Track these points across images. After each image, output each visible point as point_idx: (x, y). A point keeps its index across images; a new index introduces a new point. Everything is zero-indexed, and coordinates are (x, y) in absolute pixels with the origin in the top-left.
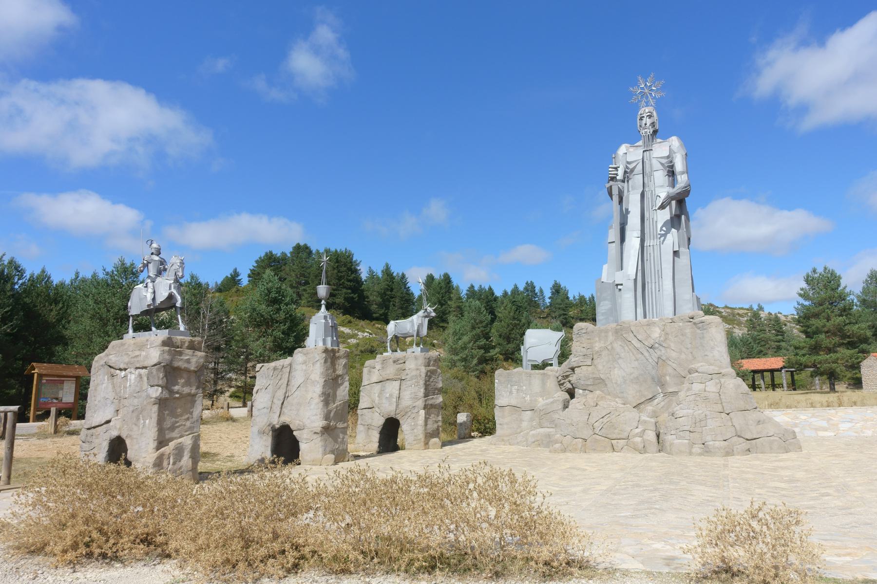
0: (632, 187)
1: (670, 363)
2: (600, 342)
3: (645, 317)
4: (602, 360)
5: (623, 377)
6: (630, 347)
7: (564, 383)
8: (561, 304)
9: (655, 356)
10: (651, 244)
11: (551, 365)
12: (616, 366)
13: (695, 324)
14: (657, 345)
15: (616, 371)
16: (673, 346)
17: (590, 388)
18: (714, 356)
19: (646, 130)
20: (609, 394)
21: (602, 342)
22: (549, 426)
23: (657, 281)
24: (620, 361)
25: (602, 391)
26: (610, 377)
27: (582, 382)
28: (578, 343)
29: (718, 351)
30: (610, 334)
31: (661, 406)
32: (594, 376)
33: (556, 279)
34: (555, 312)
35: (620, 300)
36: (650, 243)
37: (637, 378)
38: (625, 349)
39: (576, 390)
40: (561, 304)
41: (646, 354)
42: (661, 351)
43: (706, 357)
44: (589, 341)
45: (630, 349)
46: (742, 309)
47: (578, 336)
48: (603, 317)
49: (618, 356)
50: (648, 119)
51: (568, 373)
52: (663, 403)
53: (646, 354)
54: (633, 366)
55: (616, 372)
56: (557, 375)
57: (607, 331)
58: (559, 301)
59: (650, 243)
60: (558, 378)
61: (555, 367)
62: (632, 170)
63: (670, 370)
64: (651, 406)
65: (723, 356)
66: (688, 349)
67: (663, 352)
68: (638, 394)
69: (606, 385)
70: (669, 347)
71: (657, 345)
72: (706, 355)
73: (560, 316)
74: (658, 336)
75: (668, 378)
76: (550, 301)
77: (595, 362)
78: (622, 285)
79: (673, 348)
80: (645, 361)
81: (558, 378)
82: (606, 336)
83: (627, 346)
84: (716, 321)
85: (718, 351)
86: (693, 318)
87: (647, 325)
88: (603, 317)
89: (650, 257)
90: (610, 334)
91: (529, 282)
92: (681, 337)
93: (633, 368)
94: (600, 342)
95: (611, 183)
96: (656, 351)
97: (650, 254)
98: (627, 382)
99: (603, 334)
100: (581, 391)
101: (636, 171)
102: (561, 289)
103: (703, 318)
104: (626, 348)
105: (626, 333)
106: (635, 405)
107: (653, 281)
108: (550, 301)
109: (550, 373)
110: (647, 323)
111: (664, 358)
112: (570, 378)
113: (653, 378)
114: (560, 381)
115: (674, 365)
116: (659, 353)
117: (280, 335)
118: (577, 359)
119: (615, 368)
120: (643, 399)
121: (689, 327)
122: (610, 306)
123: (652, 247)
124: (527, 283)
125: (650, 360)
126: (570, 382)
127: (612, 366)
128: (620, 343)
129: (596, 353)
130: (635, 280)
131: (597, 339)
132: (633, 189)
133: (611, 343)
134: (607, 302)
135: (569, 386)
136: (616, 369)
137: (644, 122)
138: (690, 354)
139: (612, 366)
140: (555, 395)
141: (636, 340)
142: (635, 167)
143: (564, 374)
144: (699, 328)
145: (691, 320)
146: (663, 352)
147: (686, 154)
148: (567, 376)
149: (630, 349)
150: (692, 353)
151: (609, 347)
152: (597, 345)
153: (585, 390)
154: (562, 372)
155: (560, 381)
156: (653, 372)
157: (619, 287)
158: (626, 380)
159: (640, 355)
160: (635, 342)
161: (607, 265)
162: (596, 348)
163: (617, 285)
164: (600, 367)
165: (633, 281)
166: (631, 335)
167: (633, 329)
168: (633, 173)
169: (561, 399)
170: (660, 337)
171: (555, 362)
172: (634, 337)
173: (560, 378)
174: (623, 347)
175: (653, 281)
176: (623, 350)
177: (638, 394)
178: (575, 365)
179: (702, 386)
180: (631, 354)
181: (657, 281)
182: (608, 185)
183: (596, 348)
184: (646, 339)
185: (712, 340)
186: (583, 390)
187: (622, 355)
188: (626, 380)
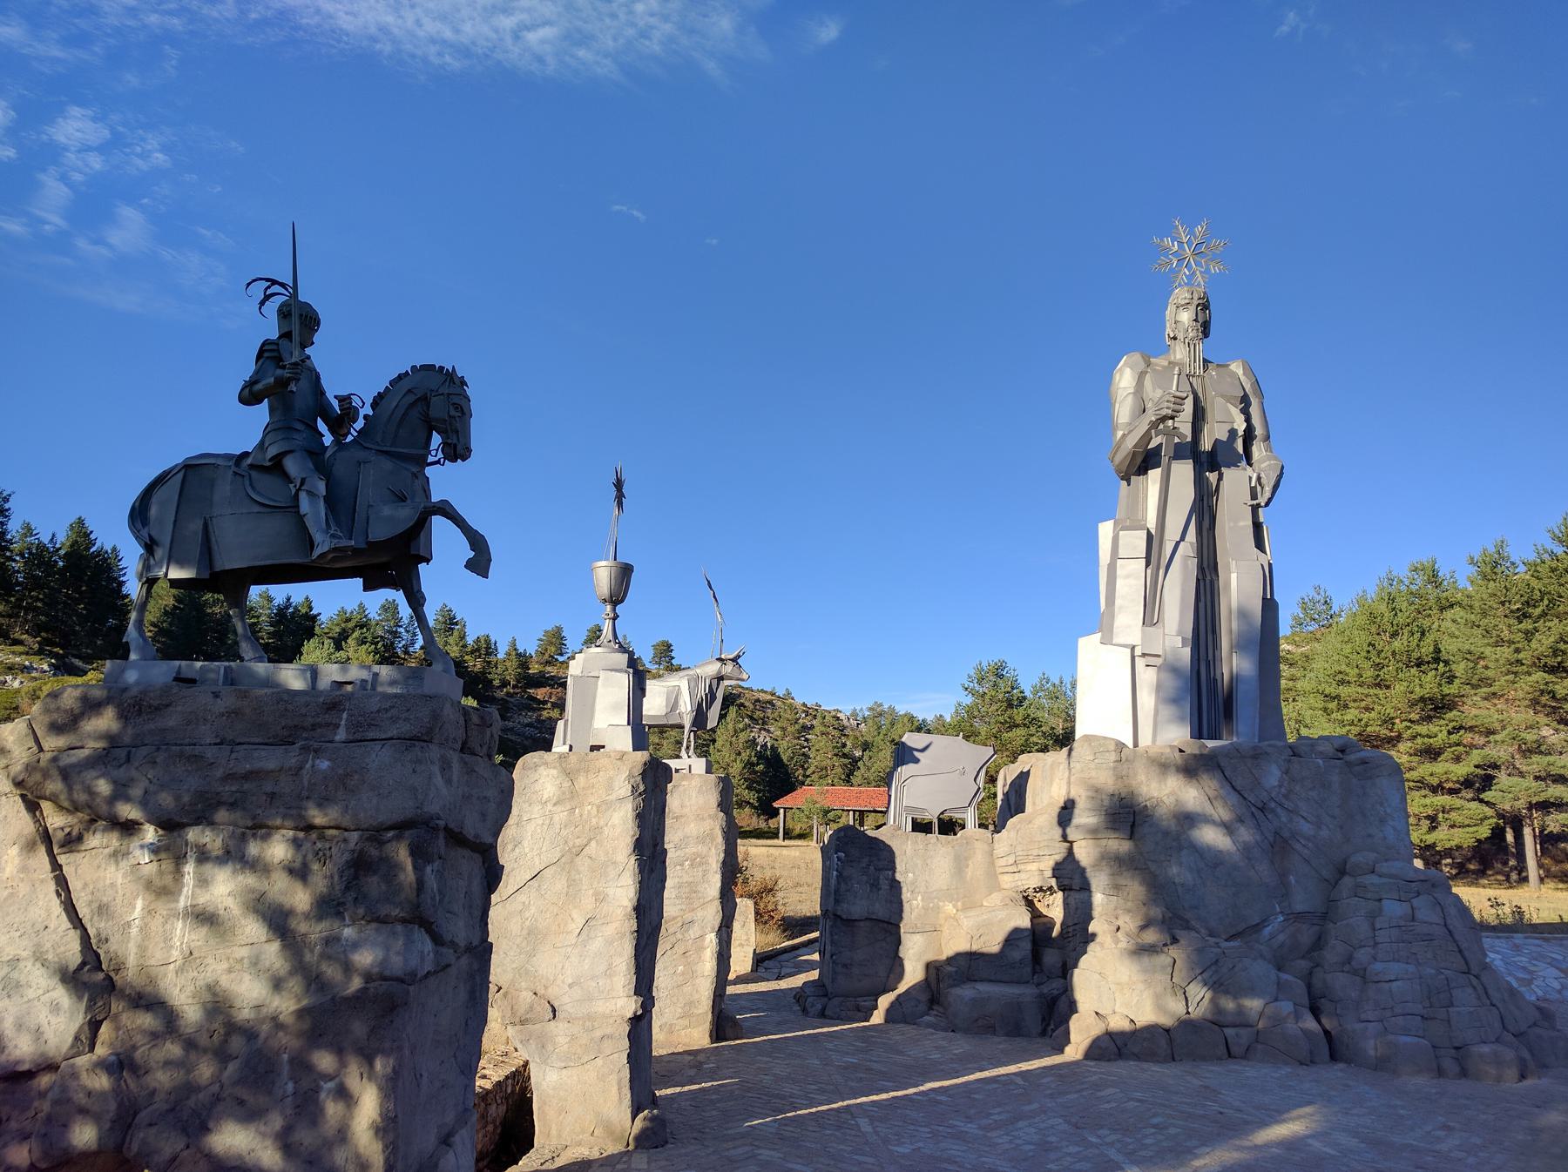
13: (1349, 764)
22: (992, 978)
29: (1394, 829)
46: (762, 691)
66: (1334, 817)
72: (1370, 836)
74: (1276, 784)
79: (1305, 814)
85: (1394, 829)
96: (1270, 816)
185: (1382, 804)
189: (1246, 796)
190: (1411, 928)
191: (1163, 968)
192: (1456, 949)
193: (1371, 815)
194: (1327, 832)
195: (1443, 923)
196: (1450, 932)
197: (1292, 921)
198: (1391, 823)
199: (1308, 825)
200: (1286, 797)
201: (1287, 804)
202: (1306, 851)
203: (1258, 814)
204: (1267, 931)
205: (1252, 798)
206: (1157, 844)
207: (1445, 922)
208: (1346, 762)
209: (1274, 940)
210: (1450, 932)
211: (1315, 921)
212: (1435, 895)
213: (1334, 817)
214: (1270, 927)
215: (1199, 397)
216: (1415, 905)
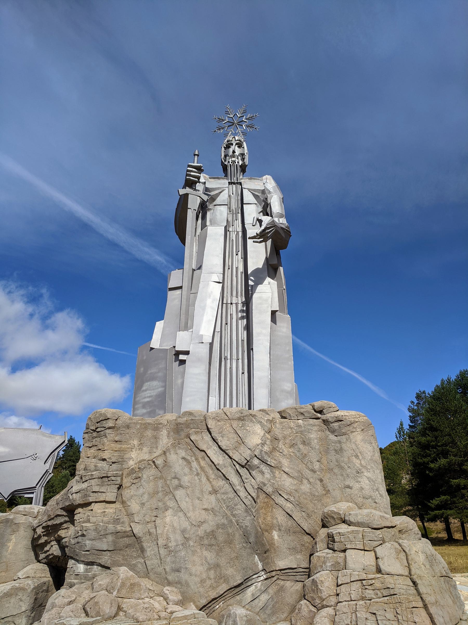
0: (210, 221)
1: (280, 501)
2: (141, 449)
3: (237, 406)
4: (141, 491)
5: (183, 531)
6: (203, 463)
7: (46, 543)
8: (72, 457)
9: (251, 484)
10: (234, 302)
11: (30, 501)
12: (171, 503)
13: (326, 422)
14: (256, 462)
15: (169, 517)
16: (285, 463)
17: (105, 559)
18: (362, 489)
19: (233, 159)
20: (147, 575)
21: (145, 449)
23: (240, 357)
24: (179, 493)
25: (132, 568)
26: (153, 530)
27: (88, 544)
28: (93, 450)
29: (368, 478)
30: (164, 432)
31: (261, 604)
32: (119, 528)
33: (72, 435)
34: (66, 463)
35: (179, 381)
36: (231, 300)
37: (212, 534)
38: (191, 468)
39: (71, 563)
40: (72, 457)
41: (234, 479)
42: (263, 473)
43: (348, 490)
44: (118, 446)
45: (201, 468)
47: (95, 434)
48: (144, 411)
49: (176, 482)
50: (237, 148)
51: (58, 521)
52: (264, 598)
53: (234, 479)
54: (205, 507)
55: (168, 520)
56: (35, 523)
57: (157, 428)
58: (71, 453)
59: (231, 300)
60: (34, 530)
61: (36, 508)
62: (213, 199)
63: (281, 518)
64: (239, 603)
65: (377, 490)
66: (314, 471)
67: (267, 476)
68: (212, 574)
69: (142, 550)
70: (278, 467)
71: (256, 462)
72: (349, 487)
73: (69, 467)
74: (260, 441)
75: (275, 535)
76: (63, 453)
77: (126, 493)
78: (187, 353)
79: (286, 470)
80: (232, 495)
81: (34, 530)
82: (156, 438)
83: (197, 459)
84: (361, 419)
85: (368, 478)
86: (321, 412)
87: (240, 419)
88: (144, 411)
89: (231, 318)
90: (164, 432)
92: (301, 446)
93: (205, 509)
94: (141, 449)
95: (188, 190)
96: (253, 473)
97: (231, 315)
98: (191, 543)
99: (149, 433)
100: (81, 568)
101: (218, 201)
102: (76, 444)
103: (339, 413)
104: (195, 464)
105: (196, 433)
106: (204, 602)
107: (235, 357)
108: (63, 453)
109: (21, 519)
110: (237, 416)
111: (269, 489)
112: (62, 533)
113: (246, 535)
114: (40, 537)
115: (288, 506)
116: (259, 478)
117: (181, 553)
118: (85, 485)
119: (166, 509)
120: (223, 588)
121: (316, 428)
122: (160, 389)
123: (234, 305)
125: (242, 494)
126: (59, 540)
127: (160, 504)
128: (182, 453)
129: (129, 475)
130: (211, 344)
131: (136, 442)
132: (213, 223)
133: (165, 453)
134: (155, 383)
135: (55, 550)
136: (170, 512)
137: (231, 150)
138: (318, 482)
139: (160, 504)
140: (20, 574)
141: (217, 448)
142: (218, 195)
143: (50, 523)
144: (333, 431)
145: (319, 415)
146: (267, 476)
147: (283, 198)
148: (57, 527)
149: (201, 468)
150: (321, 480)
151: (159, 462)
152: (134, 454)
153: (92, 563)
154: (45, 518)
155: (40, 537)
156: (247, 522)
157: (182, 357)
158: (187, 539)
159: (222, 482)
160: (213, 452)
161: (162, 322)
162: (131, 463)
163: (178, 353)
164: (134, 506)
165: (208, 346)
166: (207, 437)
167: (211, 424)
168: (215, 203)
169: (30, 584)
170: (263, 444)
171: (39, 494)
172: (211, 443)
173: (40, 531)
174: (188, 462)
175: (235, 357)
176: (187, 470)
177: (212, 574)
178: (77, 499)
179: (369, 559)
180: (204, 479)
181: (240, 357)
182: (182, 192)
183: (131, 463)
184: (235, 448)
185: (357, 456)
186: (88, 564)
187: (186, 480)
188: (187, 539)
189: (231, 455)
190: (370, 582)
191: (441, 573)
192: (420, 604)
193: (349, 467)
194: (308, 486)
195: (407, 573)
196: (414, 583)
197: (275, 578)
198: (368, 475)
199: (291, 480)
200: (269, 454)
201: (270, 461)
202: (289, 505)
203: (243, 471)
204: (250, 592)
205: (236, 456)
206: (143, 504)
207: (410, 573)
208: (324, 420)
209: (256, 601)
210: (414, 583)
211: (298, 578)
212: (400, 541)
213: (314, 471)
214: (253, 588)
215: (241, 160)
216: (379, 555)
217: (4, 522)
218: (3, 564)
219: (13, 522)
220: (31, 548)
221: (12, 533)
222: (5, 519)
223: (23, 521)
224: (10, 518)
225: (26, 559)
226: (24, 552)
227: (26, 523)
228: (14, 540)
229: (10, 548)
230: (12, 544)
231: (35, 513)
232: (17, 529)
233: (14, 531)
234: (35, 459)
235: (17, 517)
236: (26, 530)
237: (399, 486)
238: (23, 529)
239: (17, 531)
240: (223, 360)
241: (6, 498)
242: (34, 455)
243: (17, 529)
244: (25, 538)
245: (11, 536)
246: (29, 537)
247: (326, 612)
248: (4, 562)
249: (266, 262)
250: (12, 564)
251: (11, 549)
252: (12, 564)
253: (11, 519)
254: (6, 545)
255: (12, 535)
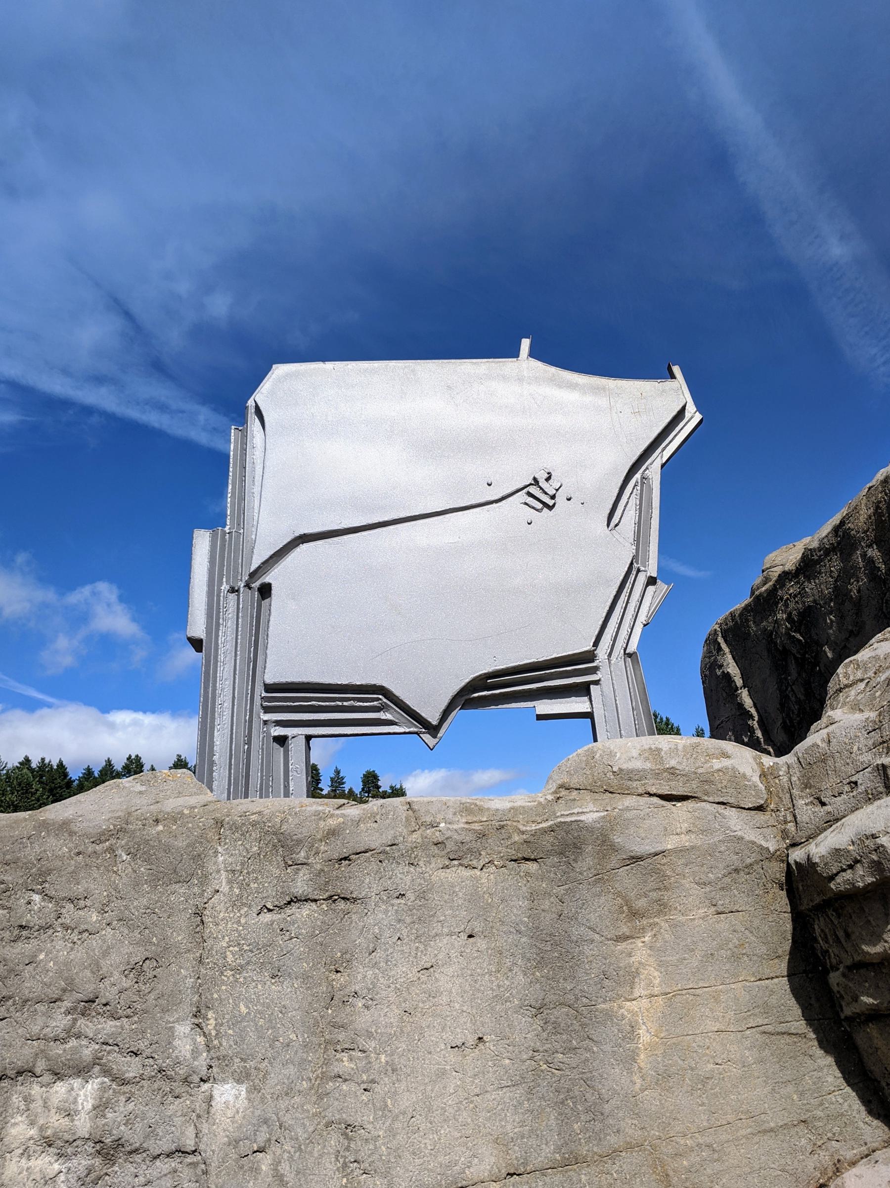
91: (133, 757)
124: (129, 758)
217: (549, 854)
218: (628, 1162)
219: (614, 848)
220: (801, 1025)
221: (625, 930)
222: (544, 831)
223: (686, 841)
224: (582, 818)
225: (795, 1119)
226: (761, 1061)
227: (711, 851)
228: (656, 976)
229: (645, 1036)
230: (645, 1002)
231: (744, 776)
232: (654, 895)
233: (634, 914)
234: (551, 503)
235: (628, 815)
236: (724, 902)
237: (436, 907)
238: (696, 890)
239: (660, 913)
240: (634, 572)
241: (431, 748)
242: (536, 481)
243: (654, 895)
244: (735, 958)
245: (622, 946)
246: (764, 949)
247: (628, 1011)
248: (630, 1147)
249: (407, 708)
250: (694, 1158)
251: (652, 1046)
252: (694, 1158)
253: (589, 829)
254: (609, 1015)
255: (625, 938)
